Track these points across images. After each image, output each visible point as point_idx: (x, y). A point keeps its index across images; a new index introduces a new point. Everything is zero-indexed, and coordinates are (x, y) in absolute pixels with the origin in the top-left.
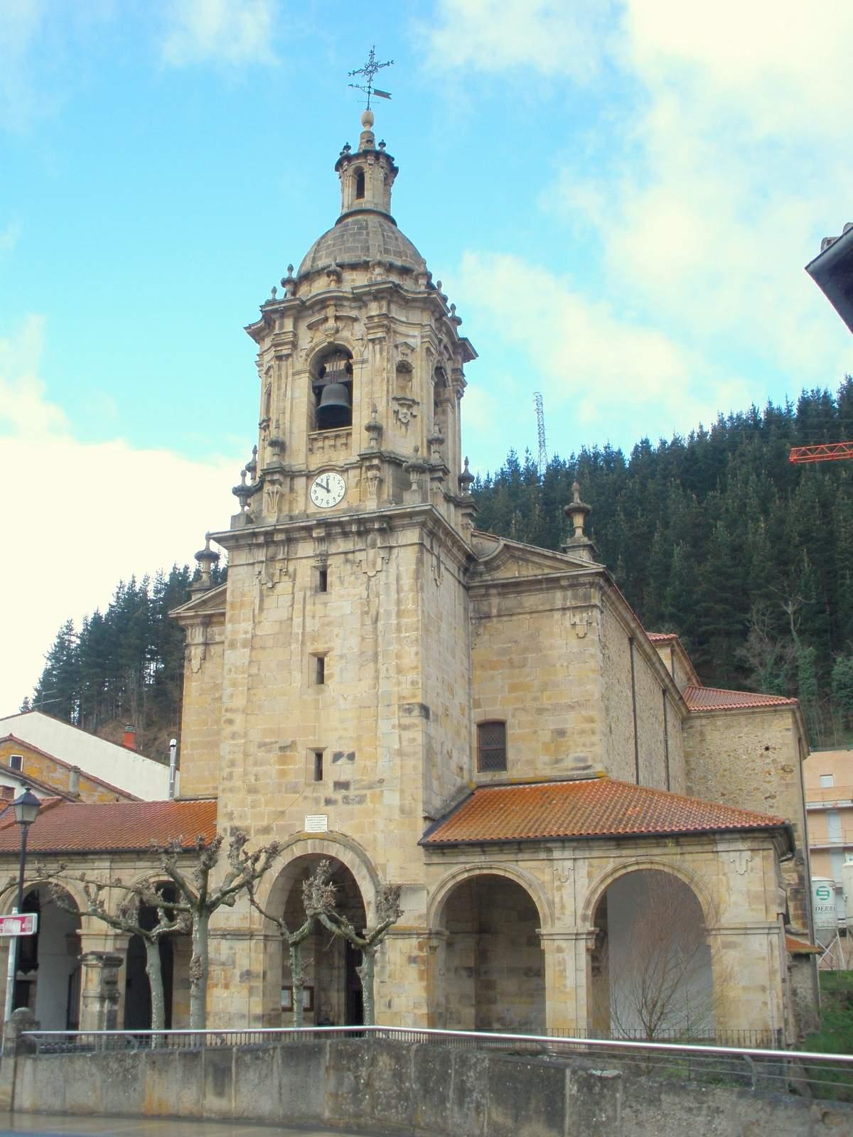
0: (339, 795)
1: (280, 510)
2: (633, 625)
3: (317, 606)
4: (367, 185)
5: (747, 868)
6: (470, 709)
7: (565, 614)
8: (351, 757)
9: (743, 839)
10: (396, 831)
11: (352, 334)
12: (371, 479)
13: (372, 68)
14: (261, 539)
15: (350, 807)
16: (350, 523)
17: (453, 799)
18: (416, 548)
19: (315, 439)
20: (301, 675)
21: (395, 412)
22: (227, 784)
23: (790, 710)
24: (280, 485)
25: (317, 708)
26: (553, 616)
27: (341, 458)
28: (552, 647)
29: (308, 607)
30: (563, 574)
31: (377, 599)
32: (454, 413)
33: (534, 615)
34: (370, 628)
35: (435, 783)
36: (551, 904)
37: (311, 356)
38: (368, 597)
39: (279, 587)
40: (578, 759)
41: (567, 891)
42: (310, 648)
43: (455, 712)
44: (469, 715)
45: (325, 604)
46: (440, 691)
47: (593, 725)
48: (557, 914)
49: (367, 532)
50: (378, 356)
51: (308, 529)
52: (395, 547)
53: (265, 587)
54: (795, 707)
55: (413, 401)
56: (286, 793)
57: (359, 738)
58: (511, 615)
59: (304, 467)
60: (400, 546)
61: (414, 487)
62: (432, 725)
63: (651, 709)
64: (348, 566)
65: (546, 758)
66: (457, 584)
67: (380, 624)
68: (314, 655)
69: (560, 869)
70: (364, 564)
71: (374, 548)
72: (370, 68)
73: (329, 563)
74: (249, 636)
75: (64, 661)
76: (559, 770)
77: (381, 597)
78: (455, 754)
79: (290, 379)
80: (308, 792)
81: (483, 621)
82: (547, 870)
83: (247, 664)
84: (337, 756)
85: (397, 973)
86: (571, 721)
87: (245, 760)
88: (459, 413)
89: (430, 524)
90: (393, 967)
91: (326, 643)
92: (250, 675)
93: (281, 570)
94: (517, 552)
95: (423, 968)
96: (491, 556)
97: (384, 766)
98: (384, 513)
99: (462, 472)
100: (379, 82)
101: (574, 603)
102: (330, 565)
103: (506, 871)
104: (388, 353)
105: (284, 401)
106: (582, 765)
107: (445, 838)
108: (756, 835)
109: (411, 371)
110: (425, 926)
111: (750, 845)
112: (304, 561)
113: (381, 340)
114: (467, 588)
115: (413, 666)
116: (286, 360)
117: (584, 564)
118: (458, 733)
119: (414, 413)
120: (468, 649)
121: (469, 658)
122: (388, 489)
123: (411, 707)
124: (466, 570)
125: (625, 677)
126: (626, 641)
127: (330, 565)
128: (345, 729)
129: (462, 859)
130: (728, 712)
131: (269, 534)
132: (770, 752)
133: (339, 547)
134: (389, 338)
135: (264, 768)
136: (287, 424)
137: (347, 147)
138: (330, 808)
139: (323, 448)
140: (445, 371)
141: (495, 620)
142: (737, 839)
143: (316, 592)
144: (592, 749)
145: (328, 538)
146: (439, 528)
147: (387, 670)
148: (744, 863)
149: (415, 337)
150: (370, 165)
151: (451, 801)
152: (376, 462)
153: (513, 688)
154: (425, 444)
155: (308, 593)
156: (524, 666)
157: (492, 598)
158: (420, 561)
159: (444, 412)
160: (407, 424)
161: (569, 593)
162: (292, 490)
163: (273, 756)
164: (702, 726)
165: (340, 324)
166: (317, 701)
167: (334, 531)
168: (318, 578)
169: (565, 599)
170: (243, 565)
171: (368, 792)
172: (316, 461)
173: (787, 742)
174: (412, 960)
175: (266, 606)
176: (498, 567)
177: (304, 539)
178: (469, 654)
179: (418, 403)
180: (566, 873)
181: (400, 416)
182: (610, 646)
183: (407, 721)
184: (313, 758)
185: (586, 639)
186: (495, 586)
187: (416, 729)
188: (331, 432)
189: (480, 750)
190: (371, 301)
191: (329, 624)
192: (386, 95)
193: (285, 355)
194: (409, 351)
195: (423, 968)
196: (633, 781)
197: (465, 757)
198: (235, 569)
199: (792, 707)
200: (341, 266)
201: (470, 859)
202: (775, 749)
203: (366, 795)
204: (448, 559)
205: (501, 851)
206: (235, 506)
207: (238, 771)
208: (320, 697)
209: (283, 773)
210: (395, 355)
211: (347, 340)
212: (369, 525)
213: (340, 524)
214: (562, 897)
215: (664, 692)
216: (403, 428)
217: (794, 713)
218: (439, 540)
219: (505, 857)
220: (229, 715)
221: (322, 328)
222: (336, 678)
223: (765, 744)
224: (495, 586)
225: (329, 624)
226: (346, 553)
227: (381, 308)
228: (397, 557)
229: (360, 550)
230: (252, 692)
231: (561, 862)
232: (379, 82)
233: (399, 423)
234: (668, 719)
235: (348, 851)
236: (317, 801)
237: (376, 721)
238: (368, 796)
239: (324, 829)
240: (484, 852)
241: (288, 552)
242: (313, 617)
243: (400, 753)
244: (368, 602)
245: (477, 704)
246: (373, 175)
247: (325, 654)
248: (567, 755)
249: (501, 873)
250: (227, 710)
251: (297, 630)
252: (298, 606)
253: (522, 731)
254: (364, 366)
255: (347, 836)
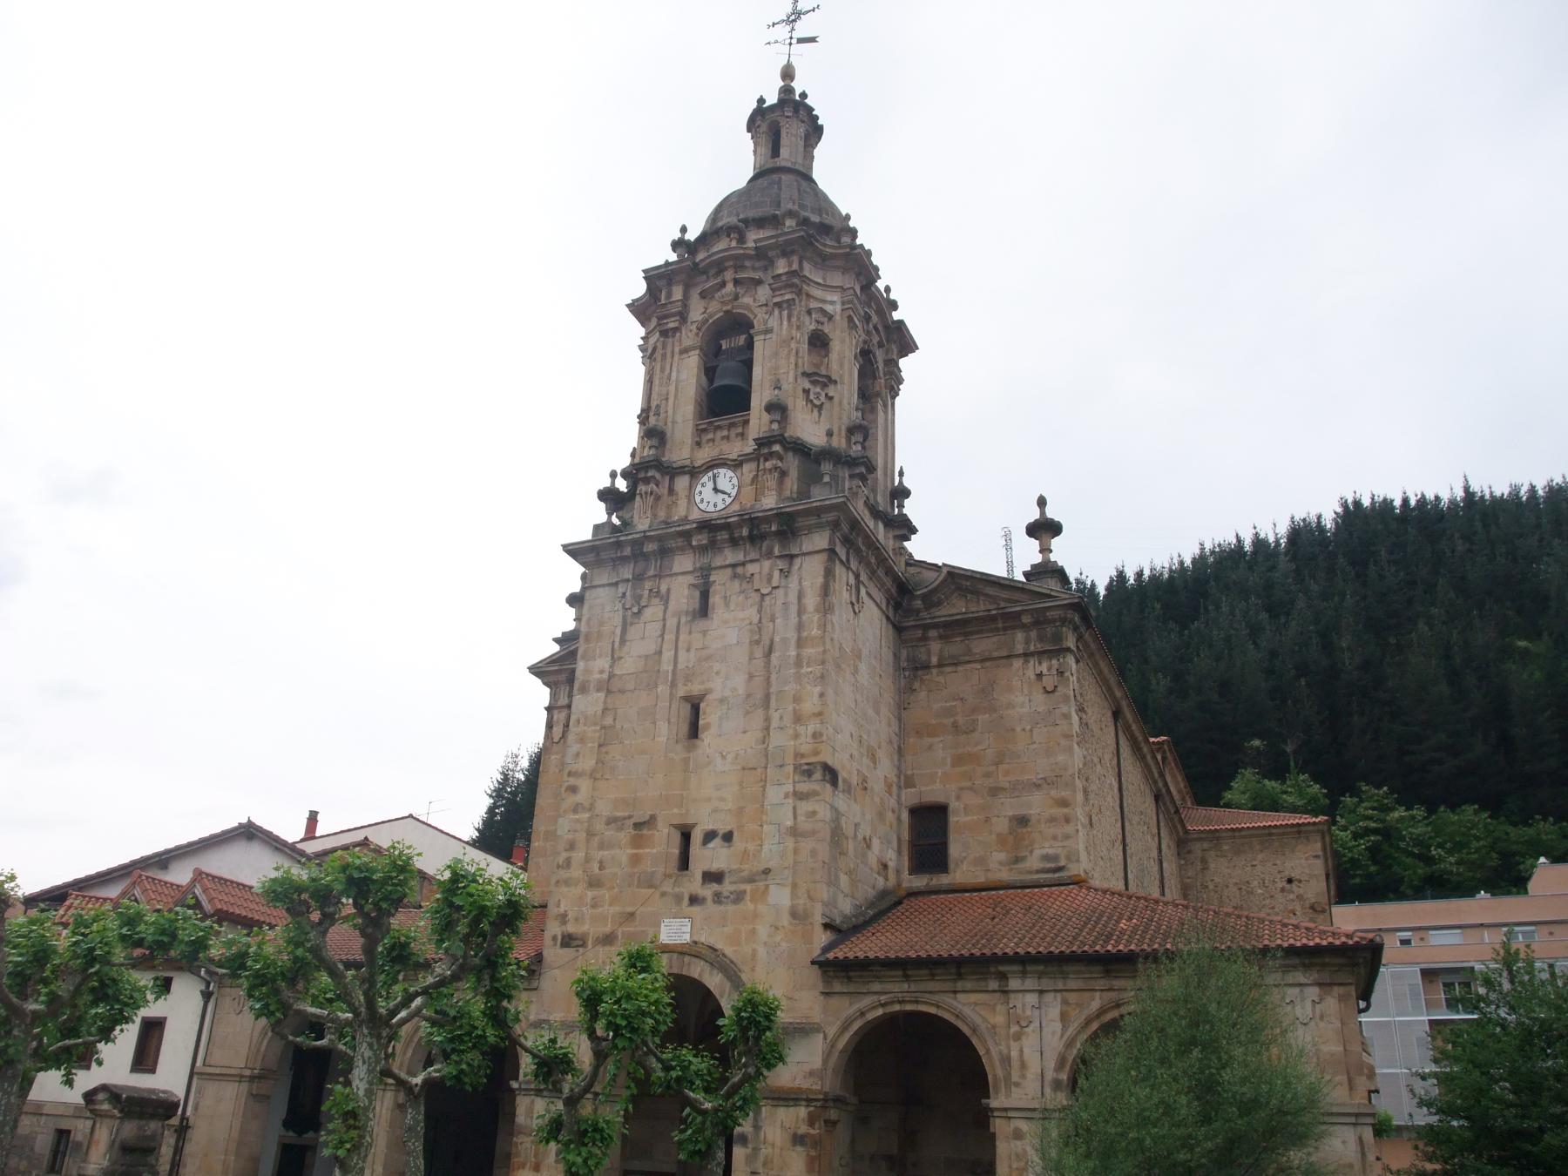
0: (707, 892)
1: (655, 516)
2: (1118, 694)
3: (693, 635)
4: (784, 141)
5: (1314, 1011)
6: (899, 787)
7: (1027, 662)
8: (728, 837)
9: (1307, 967)
10: (784, 944)
11: (755, 300)
12: (770, 470)
13: (795, 16)
14: (627, 551)
15: (722, 908)
16: (739, 525)
17: (871, 905)
18: (824, 557)
19: (704, 430)
20: (667, 729)
21: (804, 390)
22: (564, 874)
23: (1318, 831)
24: (657, 485)
25: (686, 770)
26: (1012, 665)
27: (735, 449)
28: (1010, 706)
29: (682, 637)
30: (1025, 608)
31: (771, 624)
32: (886, 413)
33: (988, 664)
34: (760, 662)
35: (844, 880)
36: (1006, 1060)
37: (704, 329)
38: (760, 621)
39: (648, 613)
40: (1046, 858)
41: (1029, 1045)
42: (681, 691)
43: (878, 786)
44: (899, 796)
45: (704, 633)
46: (855, 753)
47: (1065, 810)
48: (1015, 1078)
49: (763, 537)
50: (785, 323)
51: (686, 535)
52: (797, 556)
53: (629, 613)
54: (1325, 828)
55: (829, 378)
56: (638, 887)
57: (740, 810)
58: (956, 664)
59: (688, 463)
60: (804, 554)
61: (826, 479)
62: (841, 795)
63: (1142, 813)
64: (737, 583)
65: (1002, 856)
66: (884, 620)
67: (774, 657)
68: (686, 699)
69: (1019, 1006)
70: (756, 577)
71: (769, 558)
72: (793, 17)
73: (712, 579)
74: (605, 676)
75: (506, 798)
76: (1021, 873)
77: (778, 621)
78: (876, 843)
79: (676, 357)
80: (668, 887)
81: (920, 673)
82: (999, 1007)
83: (600, 712)
84: (710, 836)
85: (775, 1161)
86: (1037, 805)
87: (588, 841)
88: (894, 414)
89: (845, 527)
90: (770, 1150)
91: (703, 683)
92: (603, 727)
93: (651, 590)
94: (964, 583)
95: (813, 1153)
96: (929, 588)
97: (772, 850)
98: (783, 510)
99: (896, 484)
100: (802, 29)
101: (1040, 647)
102: (714, 581)
103: (938, 1007)
104: (799, 319)
105: (668, 384)
106: (1053, 865)
107: (851, 955)
108: (1327, 960)
109: (828, 344)
110: (819, 1088)
111: (1317, 976)
112: (680, 578)
113: (790, 303)
114: (899, 629)
115: (816, 711)
116: (673, 336)
117: (1052, 593)
118: (881, 815)
119: (830, 394)
120: (899, 708)
121: (900, 720)
122: (792, 484)
123: (811, 767)
124: (897, 606)
125: (1108, 756)
126: (1109, 714)
127: (714, 581)
128: (722, 799)
129: (876, 987)
130: (1237, 834)
131: (638, 544)
132: (1294, 886)
133: (726, 559)
134: (800, 301)
135: (613, 852)
136: (670, 412)
137: (761, 101)
138: (696, 909)
139: (713, 440)
140: (875, 357)
141: (934, 671)
142: (1294, 967)
143: (694, 618)
144: (1065, 844)
145: (712, 547)
146: (858, 535)
147: (781, 718)
148: (1308, 1004)
149: (834, 303)
150: (788, 117)
151: (867, 908)
152: (777, 448)
153: (958, 760)
154: (843, 433)
155: (683, 620)
156: (972, 731)
157: (931, 642)
158: (829, 573)
159: (873, 410)
160: (820, 407)
161: (1033, 634)
162: (671, 491)
163: (624, 836)
164: (1203, 850)
165: (740, 290)
166: (686, 761)
167: (719, 538)
168: (697, 600)
169: (1027, 641)
170: (603, 586)
171: (748, 887)
172: (703, 456)
173: (1316, 872)
174: (798, 1140)
175: (628, 637)
176: (939, 603)
177: (682, 549)
178: (900, 714)
179: (836, 382)
180: (1028, 1013)
181: (812, 397)
182: (1089, 711)
183: (804, 787)
184: (677, 838)
185: (1056, 693)
186: (935, 626)
187: (817, 798)
188: (724, 421)
189: (913, 844)
190: (778, 257)
191: (708, 658)
192: (812, 40)
193: (672, 329)
194: (826, 319)
195: (813, 1153)
196: (1121, 886)
197: (890, 851)
198: (593, 591)
199: (1320, 827)
200: (746, 221)
201: (888, 987)
202: (1300, 881)
203: (745, 892)
204: (872, 584)
205: (932, 977)
206: (599, 513)
207: (578, 856)
208: (691, 755)
209: (635, 860)
210: (807, 323)
211: (748, 307)
212: (764, 527)
213: (727, 527)
214: (1021, 1051)
215: (1157, 798)
216: (816, 411)
217: (1323, 838)
218: (858, 551)
219: (932, 986)
220: (572, 781)
221: (718, 295)
222: (713, 730)
223: (1286, 874)
224: (935, 626)
225: (708, 658)
226: (734, 566)
227: (790, 265)
228: (800, 569)
229: (752, 561)
230: (604, 749)
231: (1020, 995)
232: (802, 29)
233: (809, 405)
234: (1162, 835)
235: (715, 972)
236: (678, 898)
237: (764, 787)
238: (748, 891)
239: (686, 938)
240: (907, 978)
241: (660, 567)
242: (688, 650)
243: (794, 832)
244: (760, 629)
245: (909, 783)
246: (792, 134)
247: (702, 697)
248: (1031, 852)
249: (933, 1010)
250: (570, 774)
251: (667, 666)
252: (670, 637)
253: (969, 818)
254: (768, 336)
255: (716, 950)
